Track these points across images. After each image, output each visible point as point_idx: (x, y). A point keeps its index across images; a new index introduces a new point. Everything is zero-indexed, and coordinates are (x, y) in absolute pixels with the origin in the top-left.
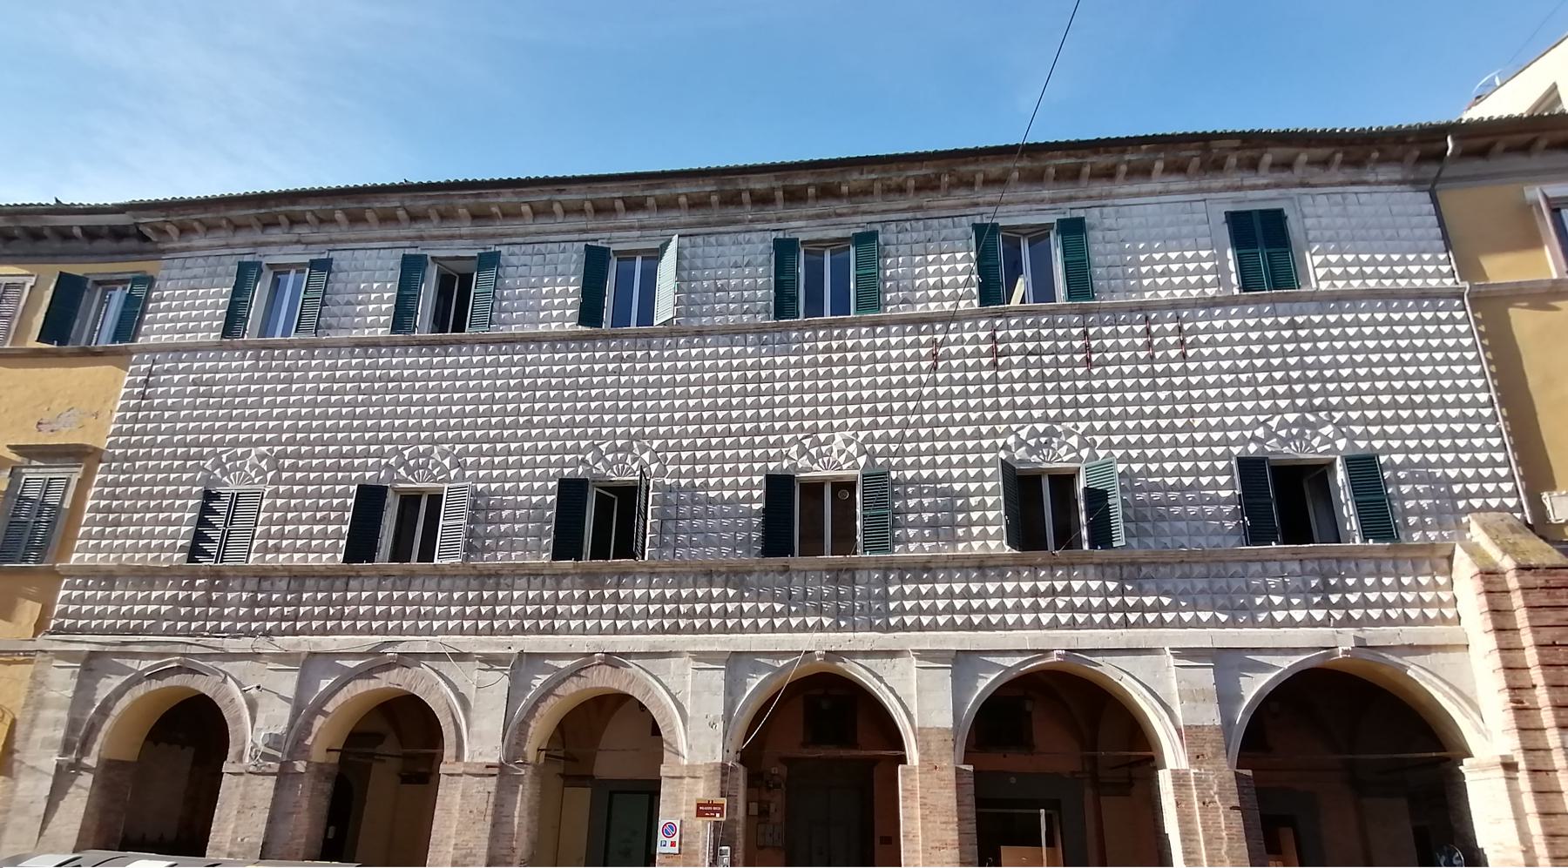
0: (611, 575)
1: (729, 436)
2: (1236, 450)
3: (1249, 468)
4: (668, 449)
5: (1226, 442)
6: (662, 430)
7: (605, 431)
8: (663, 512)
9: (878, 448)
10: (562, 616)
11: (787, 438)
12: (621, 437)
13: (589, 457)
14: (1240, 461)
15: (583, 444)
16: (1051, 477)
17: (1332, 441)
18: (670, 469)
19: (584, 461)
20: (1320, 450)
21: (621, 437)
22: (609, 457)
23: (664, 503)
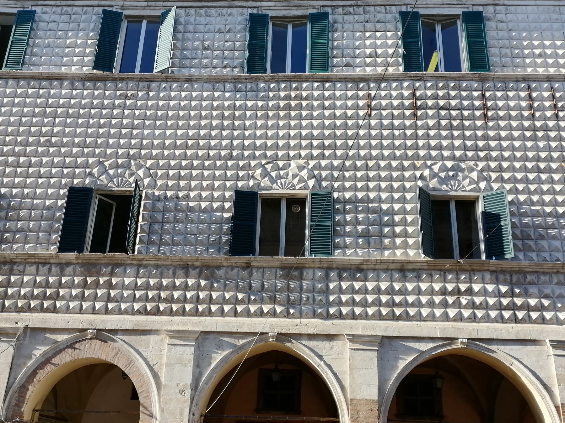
0: (106, 265)
4: (158, 167)
6: (154, 152)
7: (109, 151)
8: (152, 217)
10: (63, 298)
11: (91, 160)
12: (122, 156)
13: (95, 171)
15: (91, 160)
16: (262, 199)
19: (91, 174)
20: (298, 187)
21: (122, 156)
22: (111, 172)
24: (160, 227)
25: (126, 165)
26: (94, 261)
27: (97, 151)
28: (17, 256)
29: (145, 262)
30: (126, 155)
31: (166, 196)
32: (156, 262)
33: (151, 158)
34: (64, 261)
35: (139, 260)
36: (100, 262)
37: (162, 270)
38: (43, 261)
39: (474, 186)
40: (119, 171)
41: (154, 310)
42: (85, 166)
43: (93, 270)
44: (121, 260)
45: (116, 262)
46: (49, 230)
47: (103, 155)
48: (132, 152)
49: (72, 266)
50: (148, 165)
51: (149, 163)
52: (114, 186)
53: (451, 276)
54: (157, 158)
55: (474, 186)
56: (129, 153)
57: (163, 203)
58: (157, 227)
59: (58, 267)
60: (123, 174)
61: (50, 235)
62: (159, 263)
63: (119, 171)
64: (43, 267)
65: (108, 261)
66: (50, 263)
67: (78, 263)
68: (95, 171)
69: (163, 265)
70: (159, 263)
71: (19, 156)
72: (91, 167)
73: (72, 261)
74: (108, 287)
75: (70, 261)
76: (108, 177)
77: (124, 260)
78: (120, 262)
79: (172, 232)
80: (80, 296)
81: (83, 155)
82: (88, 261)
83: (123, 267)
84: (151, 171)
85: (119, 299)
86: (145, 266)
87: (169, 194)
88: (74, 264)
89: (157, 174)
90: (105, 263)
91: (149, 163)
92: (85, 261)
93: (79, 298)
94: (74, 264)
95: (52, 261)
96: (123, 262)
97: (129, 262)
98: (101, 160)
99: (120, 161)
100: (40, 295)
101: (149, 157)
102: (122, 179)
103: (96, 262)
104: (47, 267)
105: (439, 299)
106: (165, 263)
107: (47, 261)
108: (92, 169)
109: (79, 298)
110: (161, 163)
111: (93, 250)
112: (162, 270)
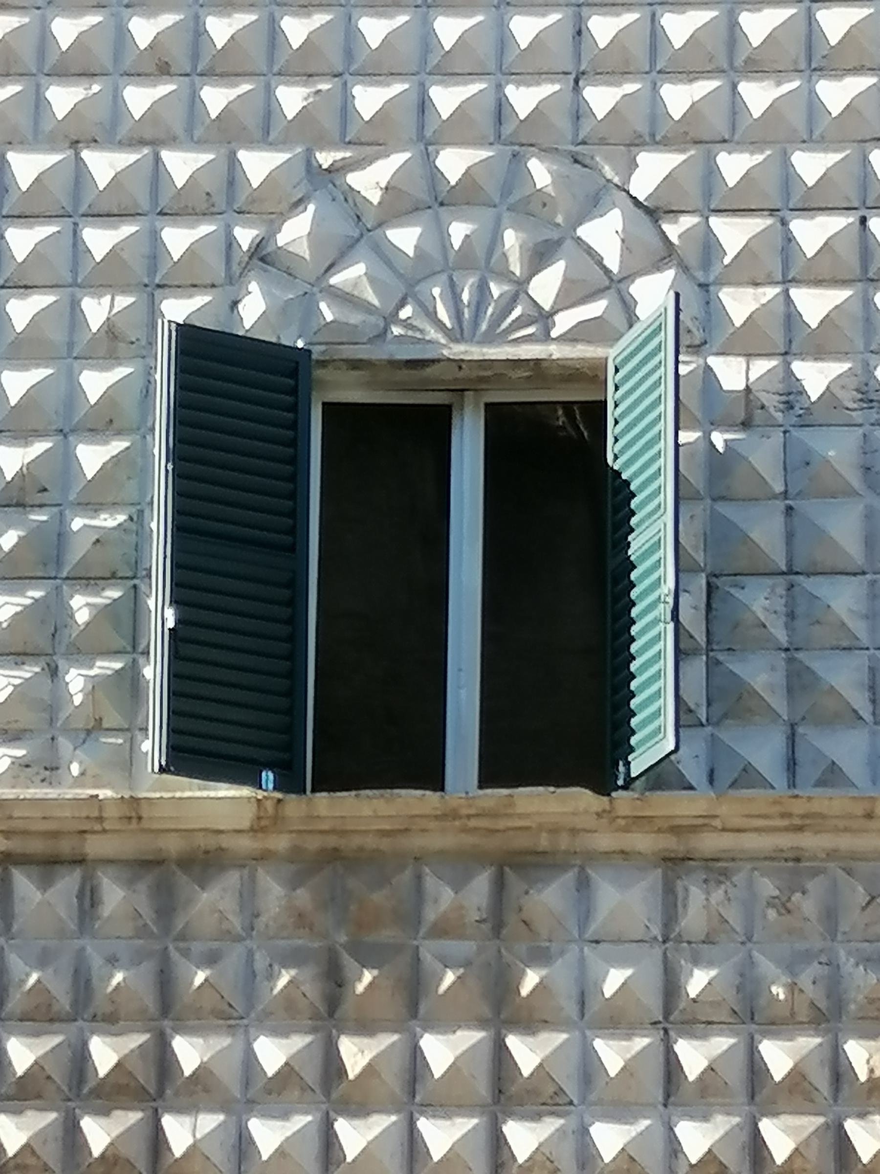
0: (459, 865)
1: (812, 140)
2: (177, 309)
3: (232, 396)
4: (717, 200)
5: (154, 276)
6: (678, 98)
7: (369, 100)
8: (721, 535)
9: (733, 234)
10: (199, 1091)
11: (258, 165)
12: (458, 130)
13: (295, 232)
14: (198, 348)
15: (258, 165)
16: (498, 419)
17: (615, 286)
18: (739, 304)
19: (263, 256)
20: (564, 322)
21: (458, 130)
22: (405, 238)
23: (710, 484)
24: (780, 604)
25: (492, 190)
26: (370, 842)
27: (292, 99)
28: (94, 815)
29: (710, 843)
30: (484, 121)
31: (792, 392)
32: (786, 841)
33: (657, 134)
34: (173, 845)
35: (676, 830)
36: (416, 842)
37: (834, 889)
38: (36, 846)
39: (595, 309)
40: (459, 232)
41: (812, 1154)
42: (220, 202)
43: (378, 897)
44: (554, 831)
45: (522, 842)
46: (44, 644)
47: (330, 123)
48: (524, 99)
49: (233, 879)
50: (642, 186)
51: (651, 171)
52: (433, 334)
53: (368, 977)
54: (696, 136)
55: (595, 309)
56: (501, 109)
57: (778, 436)
58: (760, 601)
59: (142, 887)
60: (480, 252)
61: (54, 672)
62: (809, 841)
63: (459, 232)
64: (45, 883)
65: (469, 840)
66: (79, 861)
67: (263, 857)
68: (295, 232)
69: (832, 855)
70: (809, 841)
71: (156, 143)
72: (271, 205)
73: (226, 842)
74: (486, 1011)
75: (211, 842)
76: (385, 274)
77: (574, 832)
78: (544, 842)
79: (864, 638)
80: (311, 1074)
81: (193, 128)
82: (332, 841)
83: (570, 877)
84: (673, 230)
85: (572, 1091)
86: (717, 868)
87: (815, 377)
88: (240, 862)
89: (710, 246)
90: (442, 854)
91: (651, 171)
92: (313, 844)
93: (305, 1088)
94: (240, 862)
95: (95, 846)
96: (564, 842)
97: (604, 841)
98: (325, 159)
99: (454, 163)
100: (50, 1070)
101: (643, 128)
102: (482, 289)
103: (385, 844)
104: (68, 882)
105: (786, 1130)
106: (845, 842)
107: (65, 847)
108: (275, 221)
109: (305, 1088)
110: (734, 166)
111: (502, 766)
112: (834, 889)
